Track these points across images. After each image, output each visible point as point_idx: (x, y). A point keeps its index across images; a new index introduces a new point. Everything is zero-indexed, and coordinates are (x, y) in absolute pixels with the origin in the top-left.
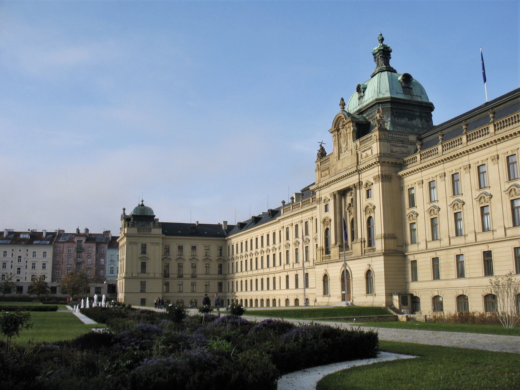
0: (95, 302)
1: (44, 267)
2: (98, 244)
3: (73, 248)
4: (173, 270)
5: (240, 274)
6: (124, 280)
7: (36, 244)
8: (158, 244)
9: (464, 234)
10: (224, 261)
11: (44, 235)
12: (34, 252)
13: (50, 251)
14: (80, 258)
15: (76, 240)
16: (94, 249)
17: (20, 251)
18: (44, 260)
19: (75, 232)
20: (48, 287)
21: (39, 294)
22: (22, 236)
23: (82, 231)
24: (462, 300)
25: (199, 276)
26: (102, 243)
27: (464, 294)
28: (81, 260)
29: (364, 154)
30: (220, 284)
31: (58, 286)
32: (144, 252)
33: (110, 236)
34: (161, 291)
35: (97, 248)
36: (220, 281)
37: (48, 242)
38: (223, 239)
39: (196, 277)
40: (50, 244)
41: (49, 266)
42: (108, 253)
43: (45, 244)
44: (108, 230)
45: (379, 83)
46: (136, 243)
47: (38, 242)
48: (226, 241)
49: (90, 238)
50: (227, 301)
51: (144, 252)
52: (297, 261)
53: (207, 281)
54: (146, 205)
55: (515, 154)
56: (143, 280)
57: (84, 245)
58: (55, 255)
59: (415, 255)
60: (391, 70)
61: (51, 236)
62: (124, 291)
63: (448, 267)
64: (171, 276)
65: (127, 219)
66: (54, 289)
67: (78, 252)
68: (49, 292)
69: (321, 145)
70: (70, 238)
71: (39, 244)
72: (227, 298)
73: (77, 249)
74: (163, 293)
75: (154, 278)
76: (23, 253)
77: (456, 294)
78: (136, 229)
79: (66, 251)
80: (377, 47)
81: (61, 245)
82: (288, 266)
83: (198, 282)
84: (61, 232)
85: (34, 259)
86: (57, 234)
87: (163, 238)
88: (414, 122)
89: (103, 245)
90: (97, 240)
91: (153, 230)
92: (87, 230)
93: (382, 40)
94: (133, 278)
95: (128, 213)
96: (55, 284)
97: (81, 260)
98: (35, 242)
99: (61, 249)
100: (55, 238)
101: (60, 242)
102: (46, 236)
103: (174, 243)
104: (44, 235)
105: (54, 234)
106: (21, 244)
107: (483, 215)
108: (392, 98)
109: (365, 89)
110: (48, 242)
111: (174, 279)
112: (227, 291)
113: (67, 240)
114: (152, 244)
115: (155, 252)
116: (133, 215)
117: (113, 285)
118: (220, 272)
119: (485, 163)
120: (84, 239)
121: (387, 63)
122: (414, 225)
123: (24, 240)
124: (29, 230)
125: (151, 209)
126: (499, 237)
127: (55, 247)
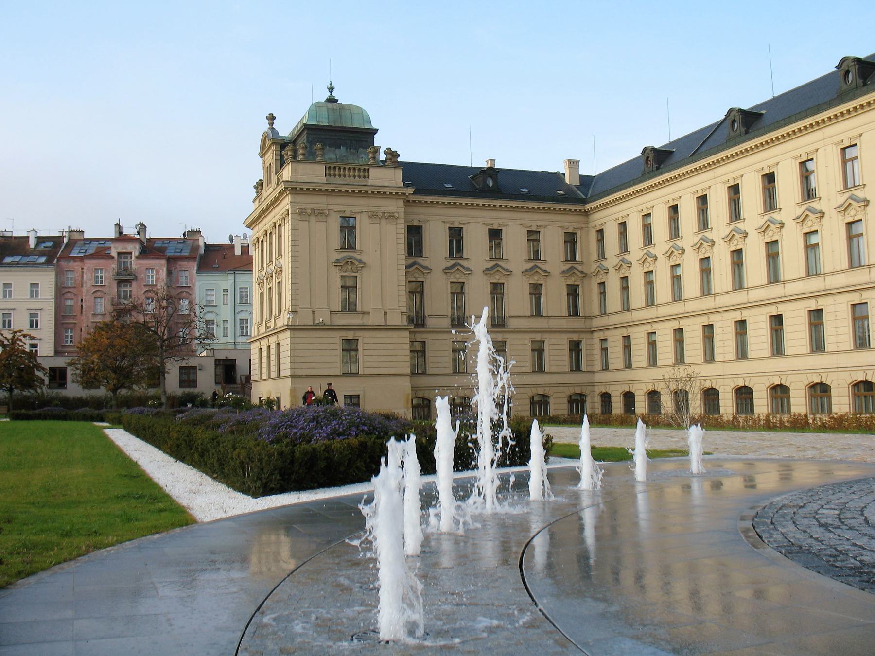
0: (97, 412)
2: (172, 261)
3: (107, 271)
6: (285, 339)
7: (10, 265)
9: (746, 286)
10: (585, 275)
11: (32, 243)
13: (46, 280)
14: (125, 297)
15: (114, 253)
16: (163, 274)
18: (34, 305)
19: (111, 234)
20: (39, 367)
21: (11, 390)
23: (130, 230)
24: (820, 391)
25: (513, 323)
26: (182, 258)
27: (747, 384)
30: (575, 347)
31: (70, 364)
32: (348, 244)
33: (201, 244)
34: (408, 371)
35: (169, 273)
37: (43, 259)
38: (578, 207)
40: (49, 262)
41: (47, 321)
42: (198, 284)
43: (35, 265)
44: (195, 228)
46: (321, 214)
47: (17, 259)
49: (151, 249)
51: (348, 244)
54: (342, 100)
55: (856, 145)
56: (350, 335)
57: (135, 264)
58: (61, 292)
59: (863, 293)
61: (50, 244)
62: (286, 370)
63: (796, 333)
65: (281, 148)
66: (58, 376)
67: (120, 282)
68: (42, 381)
70: (100, 250)
71: (18, 264)
73: (118, 274)
74: (413, 374)
77: (733, 386)
78: (320, 169)
81: (77, 265)
83: (510, 339)
84: (76, 236)
86: (66, 240)
87: (407, 202)
89: (184, 263)
90: (170, 253)
91: (374, 172)
92: (142, 227)
95: (286, 129)
96: (60, 362)
98: (8, 260)
99: (77, 275)
100: (56, 251)
101: (75, 259)
102: (37, 246)
104: (32, 243)
105: (57, 241)
107: (850, 238)
110: (43, 259)
112: (598, 367)
113: (91, 251)
114: (374, 216)
116: (307, 128)
117: (226, 360)
119: (813, 156)
120: (135, 249)
122: (678, 269)
126: (832, 287)
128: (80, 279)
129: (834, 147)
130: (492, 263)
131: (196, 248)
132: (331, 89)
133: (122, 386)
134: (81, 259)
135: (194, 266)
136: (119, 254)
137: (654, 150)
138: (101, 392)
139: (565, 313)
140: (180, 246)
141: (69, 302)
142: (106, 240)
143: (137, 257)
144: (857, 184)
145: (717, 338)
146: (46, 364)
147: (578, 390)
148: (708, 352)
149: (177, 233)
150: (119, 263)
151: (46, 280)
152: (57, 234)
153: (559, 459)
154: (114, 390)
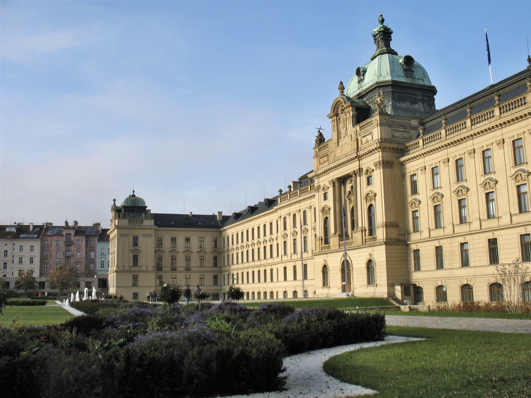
1: (31, 262)
2: (88, 237)
3: (62, 241)
4: (167, 263)
5: (236, 266)
6: (115, 273)
7: (22, 238)
8: (150, 236)
9: (468, 221)
10: (220, 253)
11: (31, 228)
12: (21, 246)
13: (37, 245)
14: (69, 251)
15: (64, 233)
16: (84, 242)
17: (6, 245)
18: (32, 254)
20: (36, 282)
21: (26, 290)
22: (8, 230)
23: (71, 224)
28: (71, 253)
29: (364, 140)
30: (215, 277)
33: (100, 229)
34: (154, 285)
35: (86, 242)
36: (215, 274)
37: (36, 236)
38: (218, 230)
39: (190, 270)
40: (38, 237)
42: (98, 246)
43: (33, 238)
44: (98, 222)
45: (380, 66)
46: (127, 235)
47: (25, 235)
48: (221, 232)
50: (223, 295)
51: (136, 244)
52: (295, 252)
53: (202, 274)
54: (137, 195)
56: (135, 274)
57: (73, 238)
58: (43, 249)
60: (392, 52)
61: (38, 229)
63: (451, 256)
64: (164, 269)
65: (117, 211)
67: (66, 246)
69: (319, 131)
70: (58, 231)
71: (26, 238)
72: (223, 292)
73: (66, 242)
75: (147, 271)
76: (9, 248)
77: (460, 284)
79: (54, 244)
80: (377, 28)
81: (49, 239)
82: (286, 257)
84: (49, 225)
85: (21, 254)
86: (45, 227)
87: (155, 230)
88: (416, 106)
89: (92, 238)
90: (87, 233)
92: (76, 223)
93: (383, 21)
94: (124, 271)
95: (119, 204)
96: (43, 279)
97: (71, 253)
98: (22, 236)
100: (42, 232)
101: (49, 236)
102: (33, 229)
103: (167, 234)
104: (31, 228)
105: (41, 227)
106: (7, 238)
108: (393, 81)
109: (365, 72)
110: (36, 236)
111: (181, 272)
112: (223, 284)
113: (55, 233)
114: (144, 236)
115: (148, 244)
118: (215, 265)
120: (73, 232)
121: (387, 45)
122: (417, 213)
123: (10, 233)
124: (15, 223)
125: (142, 199)
127: (42, 241)
128: (50, 244)
129: (509, 140)
130: (186, 249)
131: (98, 231)
132: (134, 192)
133: (64, 288)
134: (51, 236)
135: (96, 239)
136: (66, 234)
137: (268, 200)
138: (57, 291)
139: (212, 265)
140: (92, 230)
141: (46, 253)
142: (61, 227)
143: (74, 236)
144: (491, 171)
145: (308, 270)
146: (38, 280)
147: (216, 292)
148: (439, 264)
149: (91, 225)
150: (66, 238)
151: (37, 245)
152: (41, 224)
153: (397, 337)
154: (61, 290)
